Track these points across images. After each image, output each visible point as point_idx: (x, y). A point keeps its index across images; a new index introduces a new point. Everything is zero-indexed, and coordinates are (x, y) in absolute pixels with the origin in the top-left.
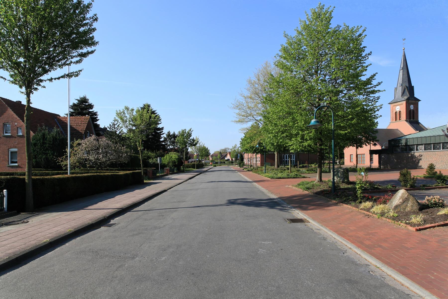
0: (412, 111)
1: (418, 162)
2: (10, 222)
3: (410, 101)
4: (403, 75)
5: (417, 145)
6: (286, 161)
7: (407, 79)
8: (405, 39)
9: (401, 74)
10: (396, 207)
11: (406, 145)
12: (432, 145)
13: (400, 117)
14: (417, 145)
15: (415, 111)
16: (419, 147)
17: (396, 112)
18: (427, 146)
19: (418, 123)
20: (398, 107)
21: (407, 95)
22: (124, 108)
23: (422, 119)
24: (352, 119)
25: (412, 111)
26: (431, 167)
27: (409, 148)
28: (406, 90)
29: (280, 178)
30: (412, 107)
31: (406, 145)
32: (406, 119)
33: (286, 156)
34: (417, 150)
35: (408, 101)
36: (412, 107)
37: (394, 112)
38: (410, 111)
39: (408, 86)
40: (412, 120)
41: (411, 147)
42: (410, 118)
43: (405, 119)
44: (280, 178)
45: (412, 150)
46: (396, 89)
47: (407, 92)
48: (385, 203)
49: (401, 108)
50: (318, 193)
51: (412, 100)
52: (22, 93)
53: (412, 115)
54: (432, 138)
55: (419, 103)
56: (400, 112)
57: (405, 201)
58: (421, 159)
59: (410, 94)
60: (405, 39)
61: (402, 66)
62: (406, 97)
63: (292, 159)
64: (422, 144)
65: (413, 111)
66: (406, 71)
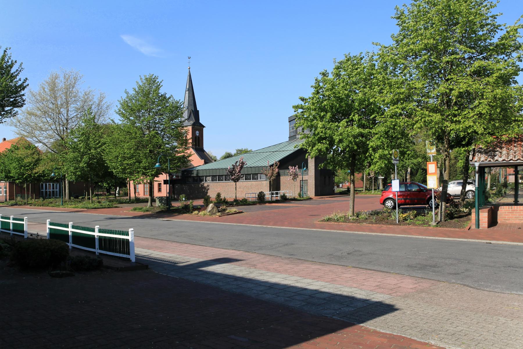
1: (207, 193)
4: (189, 97)
5: (206, 176)
6: (53, 192)
9: (187, 95)
10: (209, 211)
11: (197, 176)
12: (218, 176)
14: (206, 176)
15: (200, 138)
16: (208, 178)
18: (214, 178)
19: (204, 151)
21: (192, 120)
23: (207, 147)
24: (178, 163)
26: (219, 195)
27: (199, 179)
31: (197, 176)
34: (206, 181)
35: (193, 125)
36: (197, 133)
38: (196, 137)
41: (202, 178)
42: (196, 145)
45: (202, 180)
47: (192, 116)
48: (204, 210)
50: (157, 213)
54: (218, 171)
55: (204, 129)
57: (213, 208)
58: (208, 189)
59: (195, 120)
61: (188, 87)
62: (192, 122)
64: (210, 176)
65: (199, 137)
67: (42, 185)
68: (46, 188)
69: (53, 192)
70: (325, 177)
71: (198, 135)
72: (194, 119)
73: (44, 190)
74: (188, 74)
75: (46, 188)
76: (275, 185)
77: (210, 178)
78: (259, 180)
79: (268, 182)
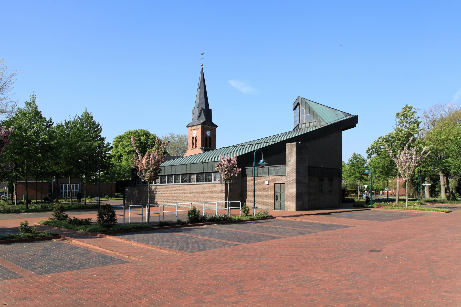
0: (208, 138)
2: (333, 226)
3: (205, 126)
5: (191, 174)
8: (203, 54)
13: (196, 144)
14: (191, 174)
15: (212, 139)
16: (218, 175)
20: (194, 132)
22: (103, 137)
25: (208, 138)
30: (208, 133)
32: (202, 146)
33: (66, 186)
36: (208, 133)
37: (191, 138)
38: (206, 137)
39: (204, 108)
40: (208, 148)
42: (206, 146)
43: (200, 146)
46: (194, 110)
47: (203, 116)
49: (197, 134)
51: (208, 125)
53: (208, 143)
55: (217, 129)
59: (206, 118)
60: (203, 54)
62: (202, 121)
63: (75, 191)
64: (194, 174)
65: (210, 138)
66: (203, 91)
67: (62, 186)
68: (66, 189)
69: (66, 192)
70: (322, 180)
71: (209, 135)
72: (204, 118)
73: (64, 191)
74: (200, 71)
75: (66, 189)
76: (237, 191)
77: (195, 177)
78: (213, 182)
79: (224, 185)
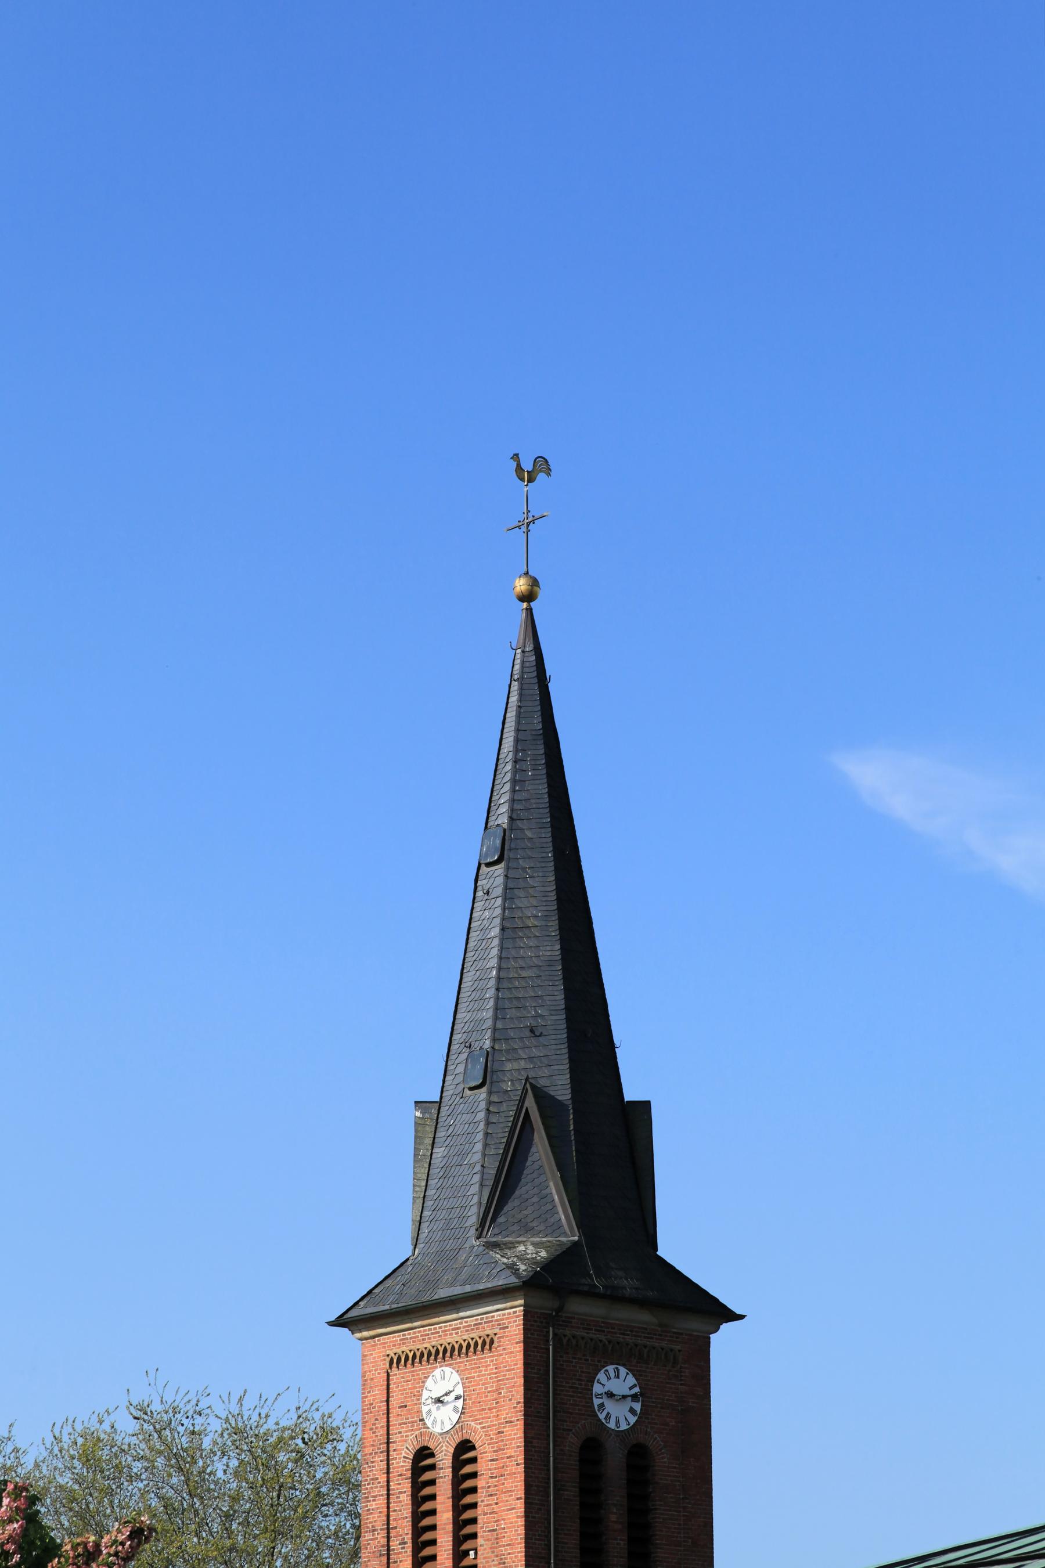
0: (615, 1461)
3: (579, 1307)
7: (555, 993)
8: (542, 465)
15: (664, 1464)
17: (423, 1456)
20: (444, 1379)
25: (615, 1461)
28: (540, 1149)
29: (504, 723)
30: (616, 1397)
35: (548, 1292)
36: (616, 1397)
38: (593, 1445)
39: (561, 1088)
44: (504, 723)
46: (431, 1112)
47: (546, 1184)
51: (614, 1297)
52: (446, 1394)
55: (722, 1342)
56: (465, 1447)
60: (542, 465)
62: (531, 1251)
65: (637, 1453)
66: (543, 882)
